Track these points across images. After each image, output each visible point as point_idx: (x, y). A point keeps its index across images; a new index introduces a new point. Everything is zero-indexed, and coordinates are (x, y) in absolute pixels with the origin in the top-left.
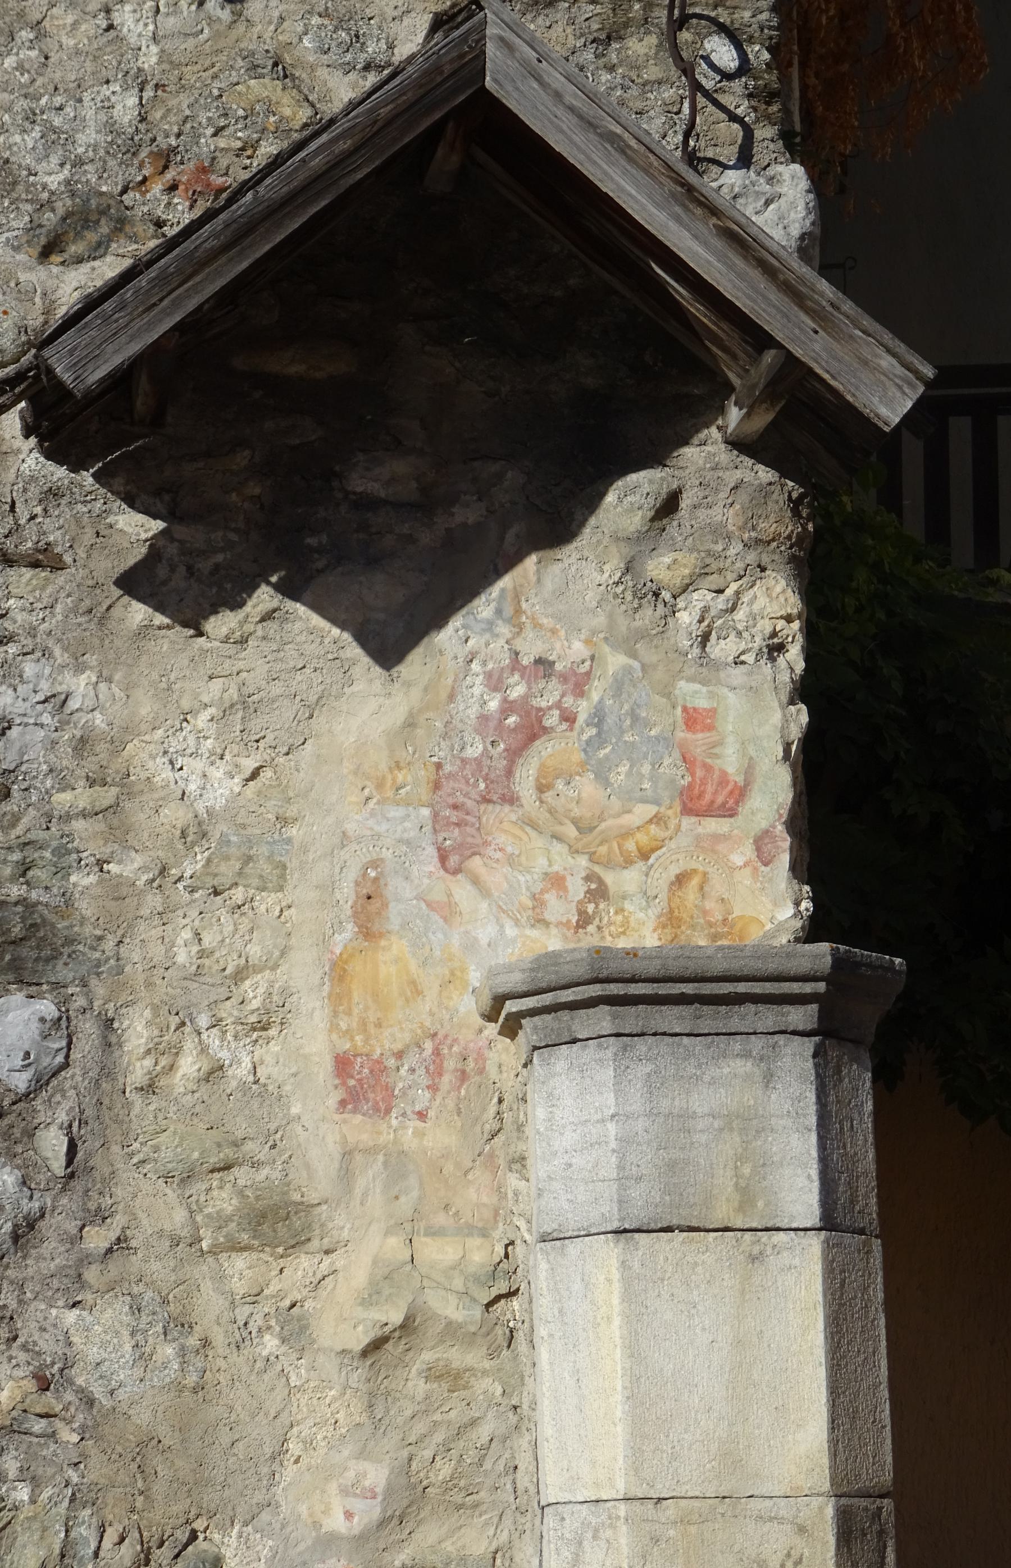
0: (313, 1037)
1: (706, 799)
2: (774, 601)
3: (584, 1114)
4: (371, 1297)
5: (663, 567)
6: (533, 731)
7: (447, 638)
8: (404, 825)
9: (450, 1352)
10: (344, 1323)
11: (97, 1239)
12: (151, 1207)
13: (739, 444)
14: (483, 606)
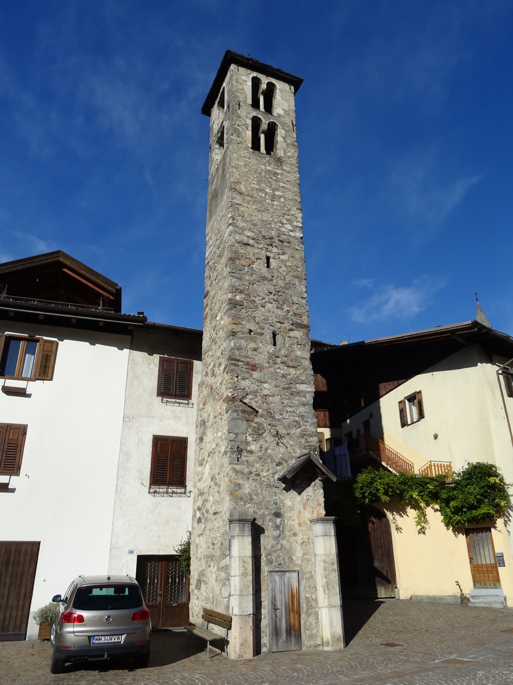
0: (296, 521)
1: (319, 505)
2: (322, 491)
3: (319, 528)
4: (301, 540)
5: (315, 488)
6: (308, 500)
7: (303, 493)
8: (301, 507)
9: (307, 543)
10: (300, 542)
11: (284, 536)
12: (287, 533)
13: (320, 480)
14: (305, 491)
